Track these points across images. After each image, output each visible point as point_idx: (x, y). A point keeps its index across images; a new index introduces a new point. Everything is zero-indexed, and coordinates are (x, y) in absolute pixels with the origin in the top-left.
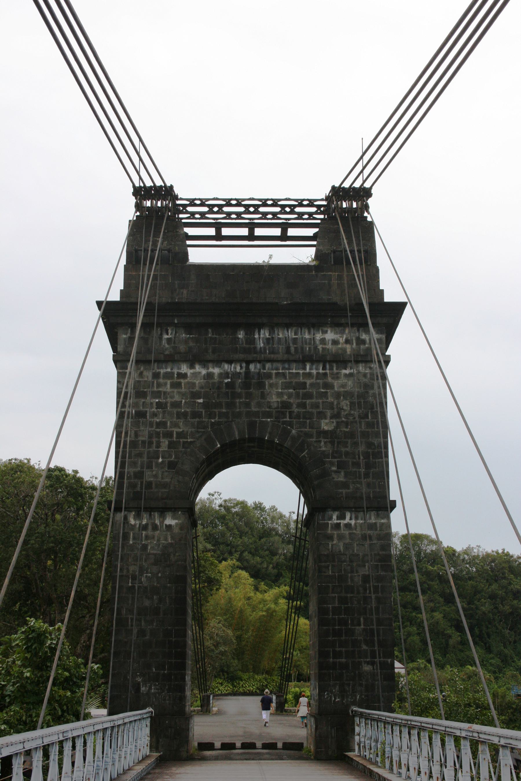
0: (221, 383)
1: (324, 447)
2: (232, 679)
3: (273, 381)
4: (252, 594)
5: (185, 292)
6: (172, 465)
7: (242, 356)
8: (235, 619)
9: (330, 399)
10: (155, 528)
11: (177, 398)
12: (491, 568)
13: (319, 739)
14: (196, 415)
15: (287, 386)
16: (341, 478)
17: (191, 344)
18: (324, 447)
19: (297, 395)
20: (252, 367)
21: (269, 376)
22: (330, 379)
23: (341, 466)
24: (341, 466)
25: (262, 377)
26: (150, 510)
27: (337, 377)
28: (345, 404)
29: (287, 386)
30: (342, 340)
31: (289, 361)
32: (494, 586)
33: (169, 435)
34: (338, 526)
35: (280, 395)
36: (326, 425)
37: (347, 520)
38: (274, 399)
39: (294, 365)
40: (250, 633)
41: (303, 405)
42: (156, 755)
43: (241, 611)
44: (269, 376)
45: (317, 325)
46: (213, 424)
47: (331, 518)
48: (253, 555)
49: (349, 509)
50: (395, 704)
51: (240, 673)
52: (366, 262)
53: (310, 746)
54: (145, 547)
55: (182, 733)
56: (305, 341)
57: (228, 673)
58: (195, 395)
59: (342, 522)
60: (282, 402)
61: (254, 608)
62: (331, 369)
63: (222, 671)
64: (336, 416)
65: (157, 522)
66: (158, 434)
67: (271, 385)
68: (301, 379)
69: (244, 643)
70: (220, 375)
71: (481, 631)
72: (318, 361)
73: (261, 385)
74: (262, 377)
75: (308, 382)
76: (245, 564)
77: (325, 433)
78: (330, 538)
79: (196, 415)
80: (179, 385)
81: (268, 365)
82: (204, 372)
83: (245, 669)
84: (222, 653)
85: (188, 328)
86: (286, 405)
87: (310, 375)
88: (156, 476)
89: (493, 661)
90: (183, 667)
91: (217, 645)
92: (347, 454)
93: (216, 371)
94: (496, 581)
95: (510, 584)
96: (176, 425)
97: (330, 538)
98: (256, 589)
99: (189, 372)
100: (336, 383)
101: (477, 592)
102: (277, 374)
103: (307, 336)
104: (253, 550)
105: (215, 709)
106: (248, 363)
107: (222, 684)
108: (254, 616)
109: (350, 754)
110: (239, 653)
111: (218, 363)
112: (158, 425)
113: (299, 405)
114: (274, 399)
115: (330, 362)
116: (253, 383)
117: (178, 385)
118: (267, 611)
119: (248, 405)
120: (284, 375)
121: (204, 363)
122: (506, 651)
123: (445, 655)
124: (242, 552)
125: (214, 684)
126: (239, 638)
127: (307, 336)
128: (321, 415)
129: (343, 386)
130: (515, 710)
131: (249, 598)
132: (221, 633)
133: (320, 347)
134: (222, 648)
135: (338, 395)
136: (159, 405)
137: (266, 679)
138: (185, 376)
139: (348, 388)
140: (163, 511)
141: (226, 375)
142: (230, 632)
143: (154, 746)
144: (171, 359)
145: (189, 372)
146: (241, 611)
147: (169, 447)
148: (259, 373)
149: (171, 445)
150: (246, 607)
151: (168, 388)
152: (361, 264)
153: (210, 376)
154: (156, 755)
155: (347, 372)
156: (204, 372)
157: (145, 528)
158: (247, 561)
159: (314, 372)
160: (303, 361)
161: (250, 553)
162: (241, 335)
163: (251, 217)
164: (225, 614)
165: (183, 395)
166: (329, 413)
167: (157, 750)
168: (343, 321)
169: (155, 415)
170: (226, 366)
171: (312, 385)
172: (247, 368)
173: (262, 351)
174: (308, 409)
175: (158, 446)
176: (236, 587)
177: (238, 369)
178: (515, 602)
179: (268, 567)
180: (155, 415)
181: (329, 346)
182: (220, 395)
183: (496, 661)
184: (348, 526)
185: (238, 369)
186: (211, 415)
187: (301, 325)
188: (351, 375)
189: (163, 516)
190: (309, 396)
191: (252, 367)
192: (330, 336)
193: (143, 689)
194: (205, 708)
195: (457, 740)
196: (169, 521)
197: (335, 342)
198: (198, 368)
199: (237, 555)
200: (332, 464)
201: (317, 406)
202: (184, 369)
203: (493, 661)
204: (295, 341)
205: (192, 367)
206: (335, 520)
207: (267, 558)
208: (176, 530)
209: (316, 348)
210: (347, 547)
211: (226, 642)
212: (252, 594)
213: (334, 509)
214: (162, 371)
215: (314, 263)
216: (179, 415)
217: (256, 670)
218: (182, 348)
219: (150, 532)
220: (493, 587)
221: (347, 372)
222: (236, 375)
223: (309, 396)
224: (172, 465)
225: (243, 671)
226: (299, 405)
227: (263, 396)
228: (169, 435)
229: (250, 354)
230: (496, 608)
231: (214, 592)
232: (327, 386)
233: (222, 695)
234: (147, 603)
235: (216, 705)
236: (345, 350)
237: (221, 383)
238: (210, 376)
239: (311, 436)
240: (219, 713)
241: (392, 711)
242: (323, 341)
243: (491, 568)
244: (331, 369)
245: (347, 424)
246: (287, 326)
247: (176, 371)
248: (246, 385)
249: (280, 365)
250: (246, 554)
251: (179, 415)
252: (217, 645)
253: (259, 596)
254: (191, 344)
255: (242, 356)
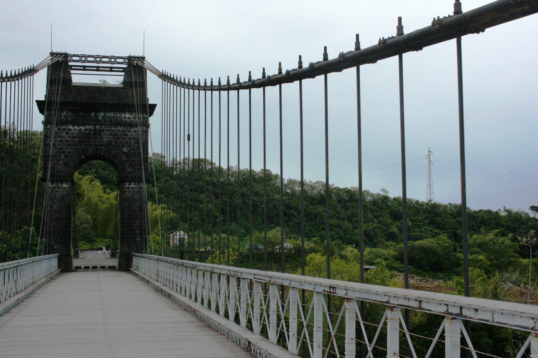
0: (85, 133)
1: (124, 158)
2: (91, 241)
3: (105, 132)
4: (102, 195)
5: (71, 96)
6: (65, 164)
7: (93, 123)
8: (93, 209)
9: (127, 140)
10: (59, 188)
11: (67, 138)
12: (243, 178)
13: (120, 264)
14: (74, 145)
15: (110, 134)
16: (130, 170)
17: (73, 117)
18: (124, 158)
19: (114, 138)
20: (97, 127)
21: (103, 130)
22: (127, 132)
23: (130, 165)
24: (130, 165)
25: (101, 131)
26: (57, 181)
27: (130, 131)
28: (132, 142)
29: (110, 134)
30: (132, 117)
31: (111, 125)
32: (244, 189)
33: (64, 153)
34: (129, 187)
35: (107, 138)
36: (125, 150)
37: (132, 186)
38: (105, 139)
39: (113, 127)
40: (101, 216)
41: (116, 142)
42: (60, 270)
43: (96, 204)
44: (103, 130)
45: (123, 111)
46: (81, 149)
47: (126, 185)
48: (104, 170)
49: (133, 182)
50: (144, 251)
51: (95, 238)
52: (142, 86)
53: (117, 266)
54: (55, 195)
55: (70, 263)
56: (117, 117)
57: (88, 238)
58: (75, 137)
59: (130, 186)
60: (109, 141)
61: (103, 202)
62: (128, 128)
63: (85, 237)
64: (129, 146)
65: (60, 186)
66: (60, 152)
67: (104, 134)
68: (116, 132)
69: (97, 222)
70: (84, 130)
71: (235, 214)
72: (123, 125)
73: (100, 134)
74: (101, 131)
75: (119, 133)
76: (99, 175)
77: (125, 153)
78: (126, 192)
79: (74, 145)
80: (68, 133)
81: (103, 126)
82: (78, 128)
83: (98, 236)
84: (85, 228)
85: (72, 111)
86: (110, 142)
87: (119, 130)
88: (59, 168)
89: (241, 231)
90: (70, 239)
91: (82, 224)
92: (133, 161)
93: (83, 128)
94: (245, 186)
95: (253, 188)
96: (68, 149)
97: (126, 192)
98: (105, 192)
99: (72, 128)
100: (129, 134)
101: (234, 192)
102: (107, 130)
103: (118, 115)
104: (104, 167)
105: (81, 256)
106: (95, 125)
107: (84, 244)
108: (103, 207)
109: (131, 269)
110: (94, 227)
111: (84, 125)
112: (60, 149)
113: (115, 142)
114: (105, 139)
115: (127, 126)
116: (97, 133)
117: (68, 133)
118: (110, 204)
119: (95, 141)
120: (109, 130)
121: (78, 125)
122: (249, 225)
123: (214, 228)
124: (97, 168)
125: (80, 244)
126: (94, 219)
127: (118, 115)
128: (124, 146)
129: (132, 135)
130: (244, 256)
131: (101, 197)
132: (84, 217)
133: (123, 120)
134: (85, 225)
135: (130, 138)
136: (60, 141)
137: (109, 241)
138: (70, 130)
139: (134, 136)
140: (62, 182)
141: (87, 130)
142: (89, 217)
143: (59, 267)
144: (66, 123)
145: (72, 128)
146: (96, 204)
147: (65, 157)
148: (100, 130)
149: (65, 157)
150: (99, 202)
151: (64, 134)
152: (140, 87)
153: (80, 130)
154: (60, 270)
155: (134, 129)
156: (78, 128)
157: (55, 188)
158: (100, 173)
159: (121, 129)
160: (117, 125)
161: (102, 169)
162: (93, 114)
163: (98, 63)
164: (87, 206)
165: (70, 137)
166: (126, 145)
167: (60, 268)
168: (132, 110)
169: (58, 145)
170: (87, 126)
171: (120, 134)
172: (95, 127)
173: (101, 121)
174: (118, 143)
175: (60, 157)
176: (93, 190)
177: (91, 127)
178: (255, 198)
179: (112, 177)
180: (58, 145)
181: (127, 119)
182: (84, 137)
183: (242, 231)
184: (132, 188)
185: (91, 127)
186: (81, 145)
187: (116, 111)
188: (135, 131)
189: (62, 184)
190: (119, 138)
191: (97, 127)
192: (127, 115)
193: (55, 247)
194: (77, 256)
195: (283, 289)
196: (65, 185)
197: (129, 118)
198: (76, 127)
199: (94, 170)
200: (127, 165)
201: (121, 142)
202: (70, 127)
203: (241, 231)
204: (114, 117)
205: (73, 126)
206: (127, 186)
207: (112, 172)
208: (67, 189)
209: (122, 120)
210: (132, 195)
211: (87, 222)
212: (102, 195)
213: (127, 182)
214: (62, 128)
215: (122, 86)
216: (68, 145)
217: (104, 237)
218: (70, 119)
219: (57, 190)
220: (243, 189)
221: (134, 129)
222: (90, 130)
223: (119, 138)
224: (65, 164)
225: (96, 237)
226: (115, 142)
227: (101, 138)
228: (64, 153)
229: (96, 121)
230: (244, 201)
231: (81, 200)
232: (126, 135)
233: (84, 250)
234: (56, 216)
235: (81, 255)
236: (133, 121)
237: (85, 133)
238: (80, 130)
239: (119, 154)
240: (83, 258)
241: (143, 253)
242: (125, 117)
243: (243, 178)
244: (128, 128)
245: (133, 150)
246: (111, 111)
247: (67, 128)
248: (95, 134)
249: (108, 127)
250: (100, 169)
251: (68, 145)
252: (82, 224)
253: (106, 196)
254: (73, 117)
255: (93, 123)
